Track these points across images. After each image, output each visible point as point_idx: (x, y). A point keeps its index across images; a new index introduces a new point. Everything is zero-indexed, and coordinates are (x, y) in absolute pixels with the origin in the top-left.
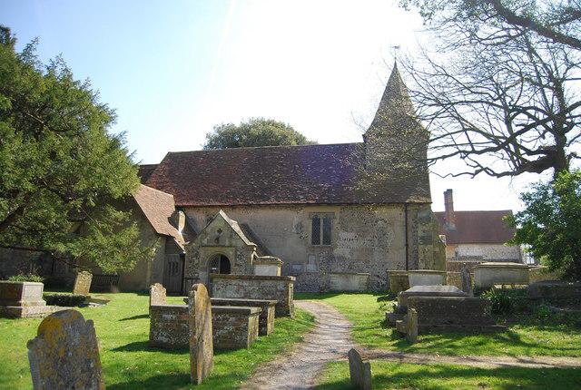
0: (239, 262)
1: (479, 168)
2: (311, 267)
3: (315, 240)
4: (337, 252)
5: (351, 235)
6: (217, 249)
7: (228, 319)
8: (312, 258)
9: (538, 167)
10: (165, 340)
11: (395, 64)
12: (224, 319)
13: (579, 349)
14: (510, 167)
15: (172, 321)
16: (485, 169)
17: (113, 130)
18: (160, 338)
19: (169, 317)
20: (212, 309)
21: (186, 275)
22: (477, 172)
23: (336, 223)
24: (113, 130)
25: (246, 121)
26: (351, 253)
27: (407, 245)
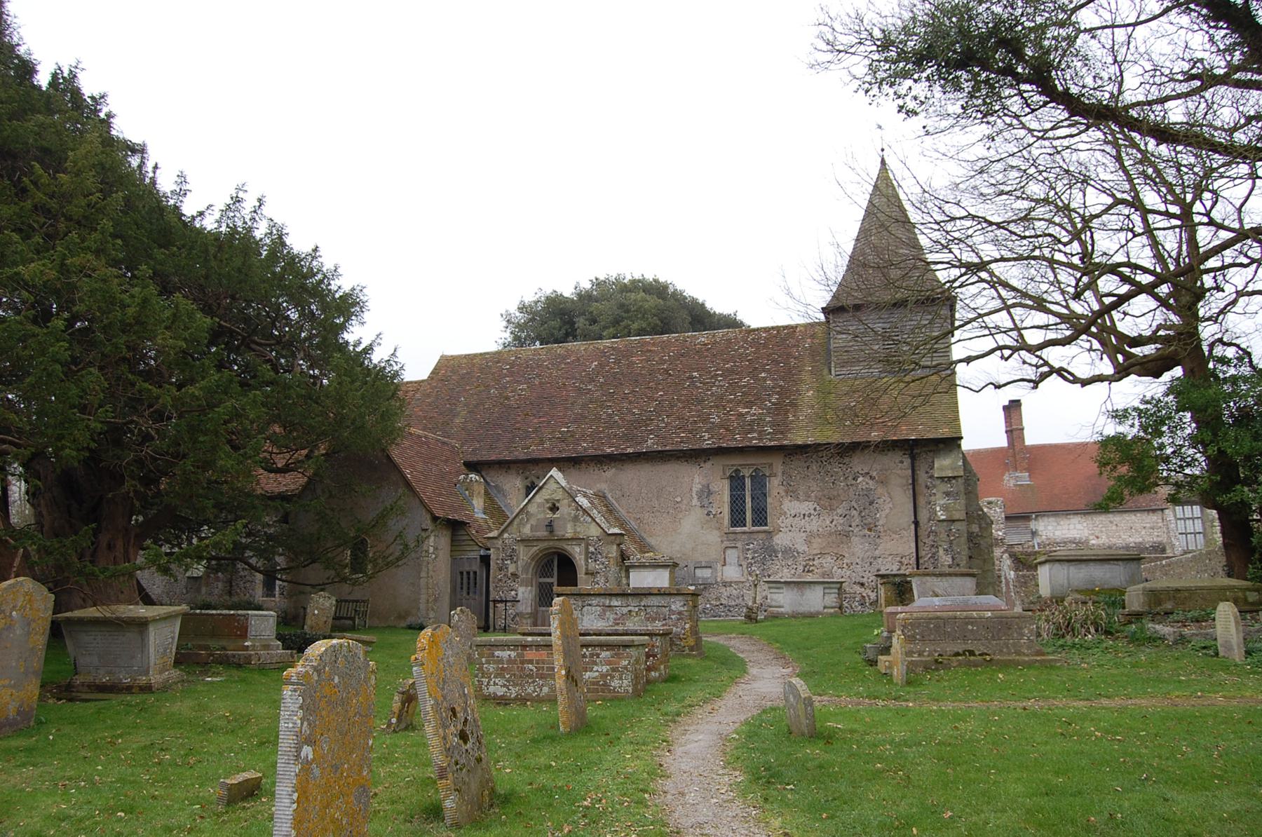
0: (592, 566)
1: (1045, 369)
2: (732, 572)
3: (737, 518)
4: (780, 540)
5: (806, 507)
6: (551, 543)
8: (732, 555)
9: (1152, 368)
10: (501, 691)
11: (883, 162)
12: (592, 655)
13: (4, 441)
14: (1107, 368)
15: (510, 661)
16: (1060, 372)
18: (492, 689)
19: (504, 654)
20: (754, 524)
22: (1044, 376)
23: (774, 486)
26: (808, 542)
27: (916, 523)
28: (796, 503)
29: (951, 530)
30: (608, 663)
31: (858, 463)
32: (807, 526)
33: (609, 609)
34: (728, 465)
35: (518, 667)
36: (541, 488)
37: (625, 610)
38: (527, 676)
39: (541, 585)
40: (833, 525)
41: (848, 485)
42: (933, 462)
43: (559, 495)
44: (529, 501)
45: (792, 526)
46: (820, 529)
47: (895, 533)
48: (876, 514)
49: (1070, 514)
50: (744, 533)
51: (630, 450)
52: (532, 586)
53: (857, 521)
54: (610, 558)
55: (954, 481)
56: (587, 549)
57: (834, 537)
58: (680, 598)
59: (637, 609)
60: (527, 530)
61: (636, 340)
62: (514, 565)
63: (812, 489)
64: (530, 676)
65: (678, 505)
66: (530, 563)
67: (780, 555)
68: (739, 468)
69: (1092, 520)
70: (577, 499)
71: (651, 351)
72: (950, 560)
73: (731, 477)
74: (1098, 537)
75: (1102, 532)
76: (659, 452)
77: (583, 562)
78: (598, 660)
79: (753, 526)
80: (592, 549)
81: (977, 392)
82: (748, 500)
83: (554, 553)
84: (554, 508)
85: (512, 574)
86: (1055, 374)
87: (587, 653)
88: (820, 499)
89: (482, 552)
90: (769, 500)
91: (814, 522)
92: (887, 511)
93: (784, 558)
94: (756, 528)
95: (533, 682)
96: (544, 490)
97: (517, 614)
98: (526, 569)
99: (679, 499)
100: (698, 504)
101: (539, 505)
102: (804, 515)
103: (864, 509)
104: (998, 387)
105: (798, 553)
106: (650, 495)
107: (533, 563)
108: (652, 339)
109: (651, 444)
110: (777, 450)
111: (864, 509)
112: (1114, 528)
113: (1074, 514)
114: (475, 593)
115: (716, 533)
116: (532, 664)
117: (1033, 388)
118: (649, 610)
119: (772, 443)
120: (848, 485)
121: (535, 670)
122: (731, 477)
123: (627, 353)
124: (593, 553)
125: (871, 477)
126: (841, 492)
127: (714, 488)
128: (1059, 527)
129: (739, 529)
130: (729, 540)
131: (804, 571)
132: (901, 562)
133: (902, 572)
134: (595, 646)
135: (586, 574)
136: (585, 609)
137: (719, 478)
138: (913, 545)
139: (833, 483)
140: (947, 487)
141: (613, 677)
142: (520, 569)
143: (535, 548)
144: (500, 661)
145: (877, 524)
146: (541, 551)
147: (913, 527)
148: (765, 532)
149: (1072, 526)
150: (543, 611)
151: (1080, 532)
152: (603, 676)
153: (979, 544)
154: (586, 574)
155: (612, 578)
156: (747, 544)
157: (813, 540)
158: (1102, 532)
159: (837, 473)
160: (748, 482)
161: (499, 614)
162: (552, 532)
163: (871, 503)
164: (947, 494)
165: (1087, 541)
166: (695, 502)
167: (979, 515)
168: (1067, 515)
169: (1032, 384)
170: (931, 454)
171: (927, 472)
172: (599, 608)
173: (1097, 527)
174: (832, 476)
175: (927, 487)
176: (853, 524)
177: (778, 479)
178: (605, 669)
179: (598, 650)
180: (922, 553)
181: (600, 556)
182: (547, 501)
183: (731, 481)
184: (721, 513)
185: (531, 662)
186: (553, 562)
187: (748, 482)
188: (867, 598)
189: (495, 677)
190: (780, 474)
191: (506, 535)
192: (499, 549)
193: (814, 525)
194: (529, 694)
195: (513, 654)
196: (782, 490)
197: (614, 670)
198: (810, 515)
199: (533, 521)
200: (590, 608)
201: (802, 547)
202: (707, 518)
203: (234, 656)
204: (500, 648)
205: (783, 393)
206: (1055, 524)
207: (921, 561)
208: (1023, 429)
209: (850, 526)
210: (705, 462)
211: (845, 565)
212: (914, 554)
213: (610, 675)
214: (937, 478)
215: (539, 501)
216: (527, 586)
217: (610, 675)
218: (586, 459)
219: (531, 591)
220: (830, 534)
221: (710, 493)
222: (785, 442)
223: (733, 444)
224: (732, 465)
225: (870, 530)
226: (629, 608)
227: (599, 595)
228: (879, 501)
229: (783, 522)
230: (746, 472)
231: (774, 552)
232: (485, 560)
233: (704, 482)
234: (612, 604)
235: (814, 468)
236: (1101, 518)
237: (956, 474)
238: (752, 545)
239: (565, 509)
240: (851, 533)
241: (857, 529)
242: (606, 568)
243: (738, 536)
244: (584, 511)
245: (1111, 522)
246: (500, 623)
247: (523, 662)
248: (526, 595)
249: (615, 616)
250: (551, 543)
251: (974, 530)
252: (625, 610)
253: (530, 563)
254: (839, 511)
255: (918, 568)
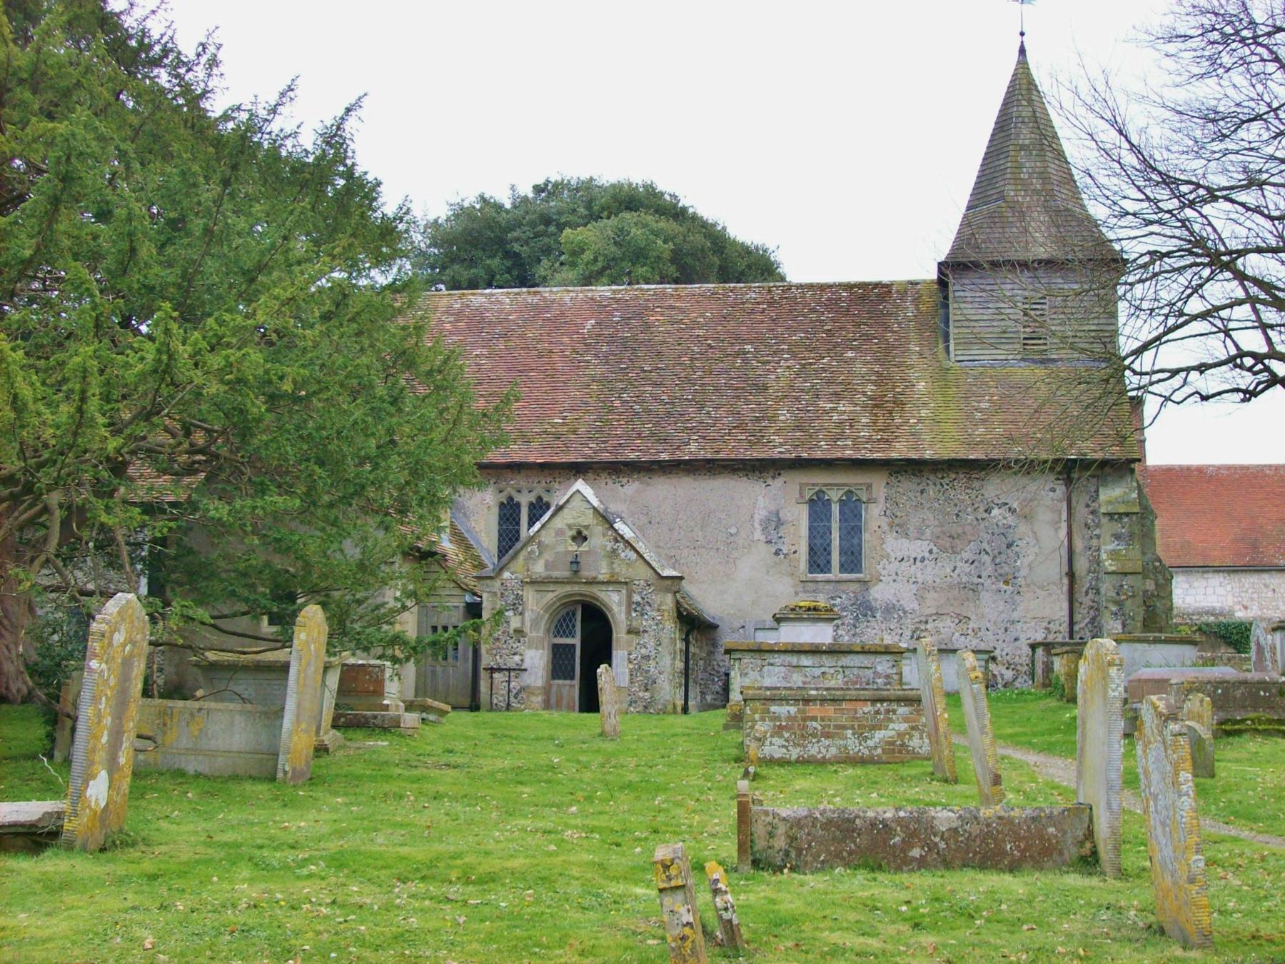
3: (818, 560)
5: (919, 548)
6: (576, 588)
7: (894, 712)
11: (1022, 51)
12: (888, 711)
17: (691, 210)
20: (843, 568)
21: (486, 660)
23: (874, 516)
24: (691, 210)
25: (526, 190)
26: (919, 597)
27: (1071, 575)
28: (904, 543)
29: (1122, 586)
30: (906, 720)
31: (993, 487)
32: (919, 575)
33: (797, 669)
34: (808, 484)
35: (799, 725)
36: (560, 508)
37: (817, 672)
38: (811, 735)
39: (556, 649)
40: (955, 575)
41: (977, 520)
42: (1097, 491)
43: (588, 519)
44: (543, 526)
45: (897, 574)
46: (938, 580)
47: (1042, 588)
48: (1015, 561)
49: (1208, 572)
50: (829, 582)
51: (665, 456)
52: (543, 649)
53: (989, 569)
54: (664, 611)
55: (1126, 520)
56: (629, 596)
57: (956, 592)
58: (888, 657)
59: (832, 671)
60: (539, 569)
61: (649, 290)
62: (518, 618)
63: (927, 522)
64: (814, 735)
65: (732, 539)
66: (543, 616)
67: (878, 615)
68: (824, 488)
69: (1240, 581)
70: (616, 526)
71: (674, 308)
72: (1120, 627)
73: (811, 502)
74: (1246, 608)
75: (1252, 599)
76: (709, 461)
77: (623, 616)
78: (894, 717)
79: (841, 572)
80: (637, 598)
81: (1178, 403)
82: (835, 535)
83: (577, 602)
84: (580, 537)
85: (515, 631)
86: (1278, 385)
87: (882, 709)
88: (938, 537)
89: (468, 598)
90: (866, 536)
91: (929, 569)
92: (1031, 557)
93: (885, 619)
94: (845, 576)
95: (818, 742)
96: (565, 510)
97: (522, 689)
98: (535, 623)
99: (733, 530)
100: (763, 538)
101: (559, 533)
102: (915, 559)
103: (1000, 553)
104: (1205, 398)
105: (905, 612)
106: (692, 524)
107: (547, 616)
108: (676, 290)
109: (694, 450)
110: (881, 465)
111: (1000, 553)
112: (1270, 594)
113: (1214, 571)
114: (456, 658)
115: (788, 581)
116: (816, 721)
117: (1243, 401)
118: (847, 672)
119: (875, 456)
120: (977, 520)
121: (820, 728)
122: (811, 502)
123: (639, 312)
124: (638, 604)
125: (1010, 509)
126: (968, 528)
127: (786, 515)
128: (1192, 591)
129: (820, 576)
130: (805, 592)
131: (912, 637)
132: (1047, 629)
133: (1048, 640)
134: (891, 701)
135: (629, 632)
136: (766, 669)
137: (794, 501)
138: (1065, 605)
139: (957, 515)
140: (1117, 528)
141: (911, 737)
142: (528, 624)
143: (551, 595)
144: (776, 718)
145: (1017, 575)
146: (560, 599)
147: (1066, 581)
148: (859, 581)
149: (1210, 591)
150: (558, 685)
151: (1220, 598)
152: (900, 735)
153: (1155, 606)
154: (629, 632)
155: (666, 640)
156: (832, 598)
157: (927, 595)
158: (1252, 599)
159: (963, 501)
160: (835, 509)
161: (495, 688)
162: (576, 572)
163: (1009, 546)
164: (1117, 537)
165: (1231, 613)
166: (758, 535)
167: (1155, 568)
168: (1204, 572)
169: (1241, 395)
170: (1094, 480)
171: (1088, 506)
172: (783, 669)
173: (1247, 592)
174: (956, 505)
175: (1087, 526)
176: (984, 574)
177: (881, 506)
178: (903, 727)
179: (894, 706)
180: (1077, 617)
181: (648, 608)
182: (570, 527)
183: (811, 508)
184: (795, 552)
185: (814, 719)
186: (574, 614)
187: (835, 509)
188: (999, 677)
189: (772, 736)
190: (882, 500)
191: (506, 575)
192: (495, 594)
193: (929, 573)
194: (813, 756)
195: (793, 710)
196: (884, 522)
197: (913, 728)
198: (923, 560)
199: (548, 556)
200: (771, 667)
201: (910, 604)
202: (776, 559)
203: (375, 717)
204: (777, 702)
205: (881, 379)
206: (1187, 586)
207: (1076, 628)
208: (1144, 441)
209: (979, 577)
210: (773, 478)
211: (970, 631)
212: (1067, 619)
213: (909, 734)
214: (1104, 514)
215: (559, 526)
216: (537, 648)
217: (909, 734)
218: (594, 466)
219: (542, 654)
220: (951, 587)
221: (780, 523)
222: (894, 455)
223: (818, 454)
224: (813, 485)
225: (1006, 583)
226: (823, 669)
227: (786, 652)
228: (1019, 543)
229: (886, 569)
230: (835, 495)
231: (871, 610)
232: (474, 610)
233: (773, 508)
234: (801, 664)
235: (931, 493)
236: (1252, 580)
237: (1129, 510)
238: (839, 600)
239: (599, 540)
240: (980, 587)
241: (989, 581)
242: (657, 624)
243: (820, 586)
244: (628, 543)
245: (1266, 586)
246: (499, 699)
247: (804, 719)
248: (536, 661)
249: (804, 679)
250: (576, 588)
251: (1148, 588)
252: (817, 672)
253: (543, 616)
254: (965, 555)
255: (1071, 637)
